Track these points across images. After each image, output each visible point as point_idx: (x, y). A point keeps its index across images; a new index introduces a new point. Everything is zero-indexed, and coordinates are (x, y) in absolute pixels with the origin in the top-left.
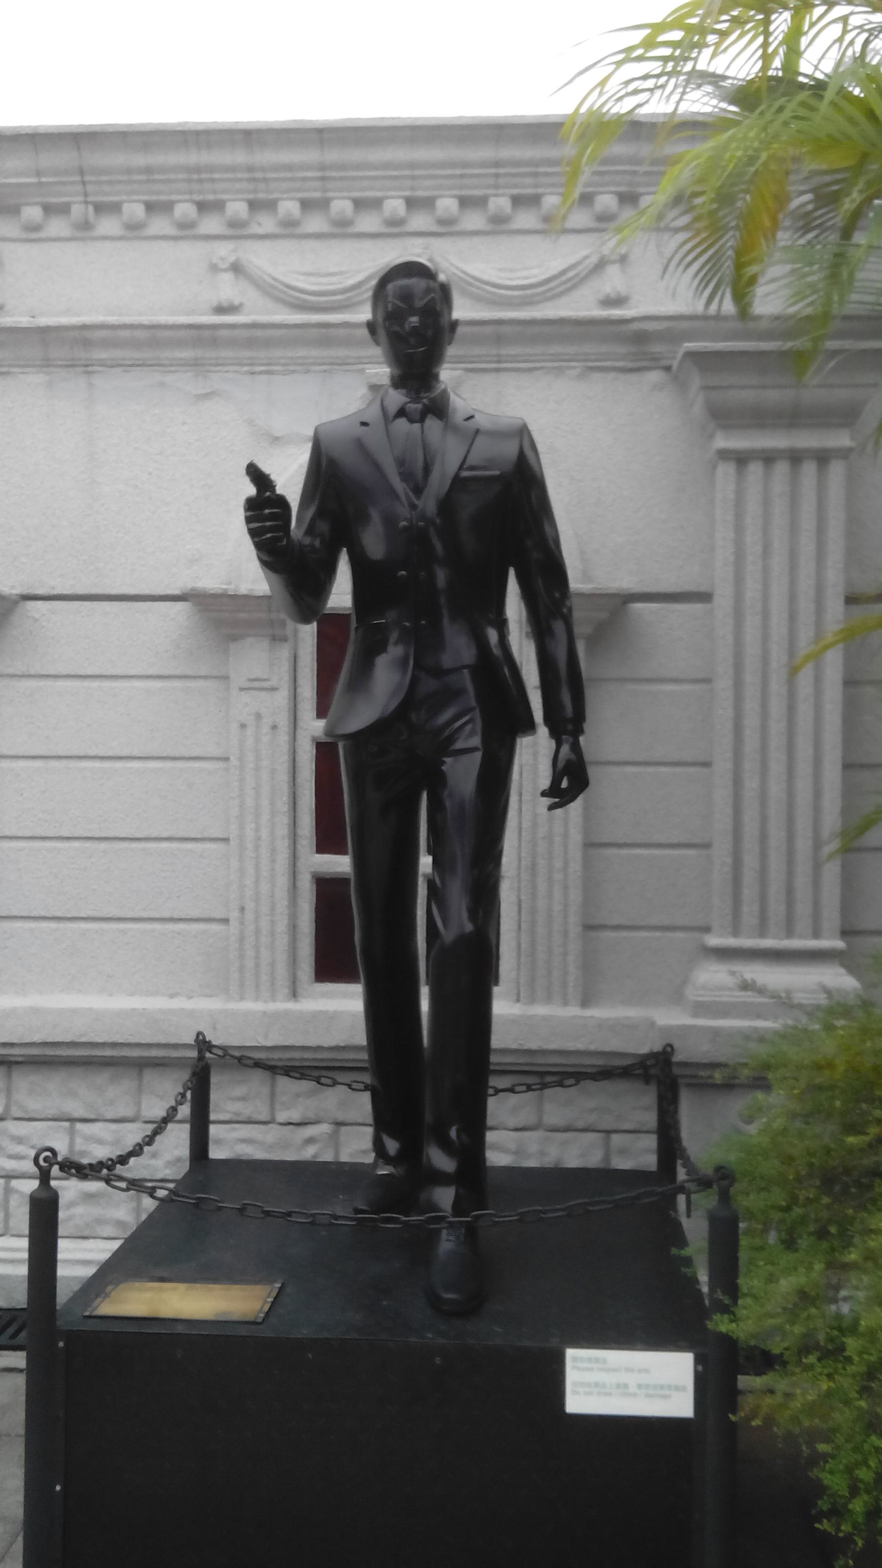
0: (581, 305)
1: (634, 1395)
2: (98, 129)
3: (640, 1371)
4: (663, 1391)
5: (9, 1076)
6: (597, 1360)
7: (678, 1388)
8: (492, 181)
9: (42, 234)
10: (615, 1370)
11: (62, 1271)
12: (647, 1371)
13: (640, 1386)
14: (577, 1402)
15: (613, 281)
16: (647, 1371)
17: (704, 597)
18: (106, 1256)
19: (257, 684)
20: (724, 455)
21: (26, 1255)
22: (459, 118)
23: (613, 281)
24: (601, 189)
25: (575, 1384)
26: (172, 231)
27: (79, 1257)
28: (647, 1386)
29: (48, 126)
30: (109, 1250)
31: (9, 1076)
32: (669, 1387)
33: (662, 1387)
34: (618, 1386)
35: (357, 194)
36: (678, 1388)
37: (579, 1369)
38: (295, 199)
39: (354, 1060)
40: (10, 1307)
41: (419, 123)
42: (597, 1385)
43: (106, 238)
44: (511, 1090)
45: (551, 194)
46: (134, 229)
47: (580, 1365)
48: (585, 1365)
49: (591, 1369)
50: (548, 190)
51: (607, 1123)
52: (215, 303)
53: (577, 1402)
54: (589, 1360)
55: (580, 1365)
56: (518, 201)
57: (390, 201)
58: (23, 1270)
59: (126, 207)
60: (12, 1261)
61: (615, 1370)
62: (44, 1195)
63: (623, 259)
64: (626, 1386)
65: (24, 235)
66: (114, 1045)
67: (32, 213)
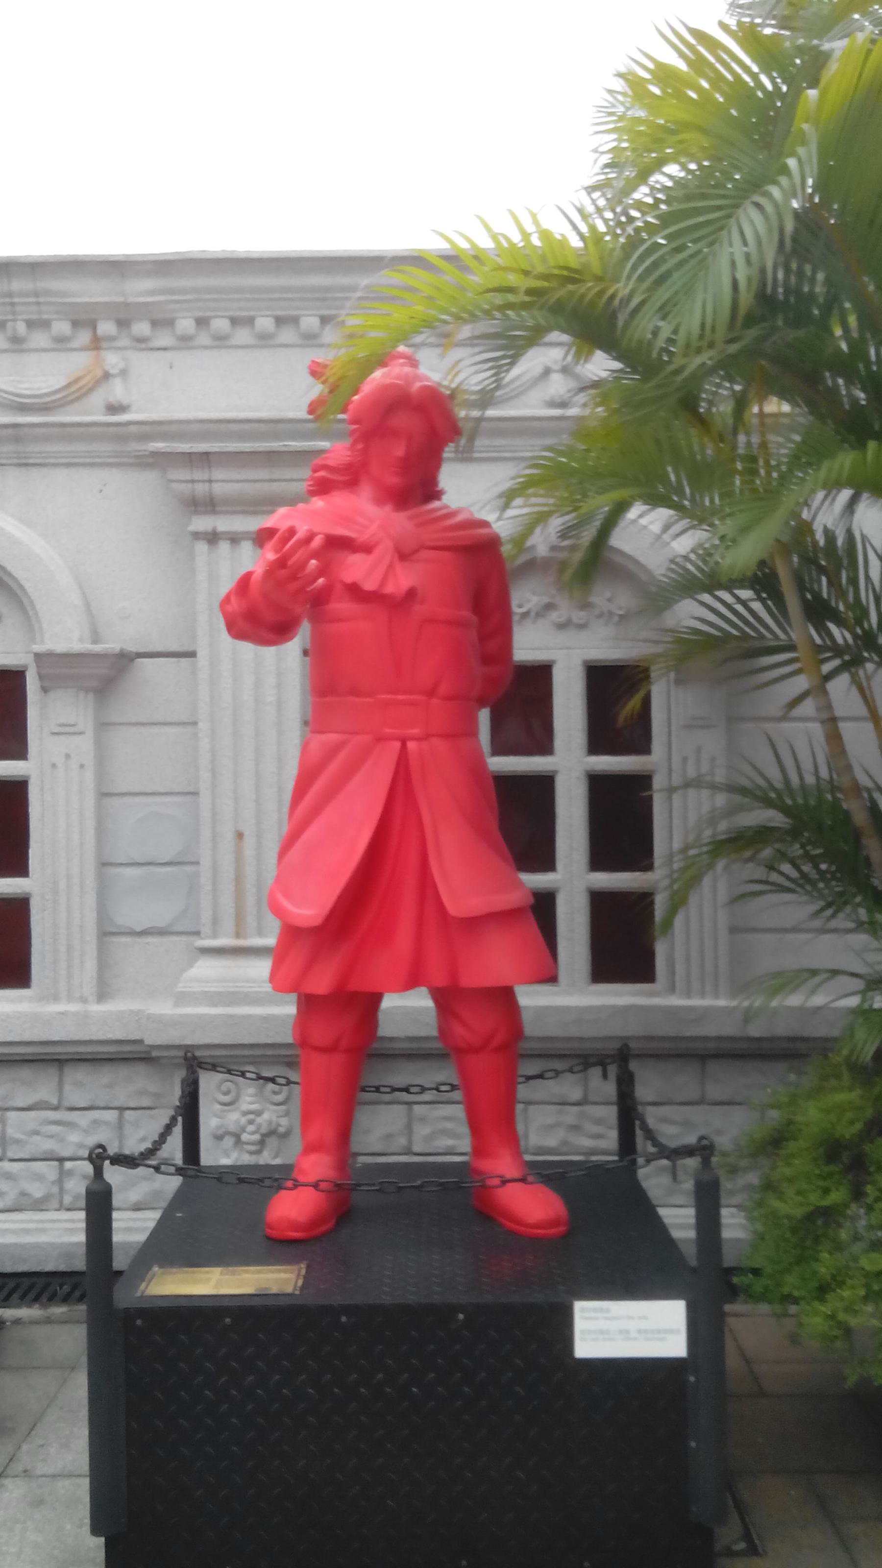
0: (91, 411)
1: (635, 1339)
2: (171, 258)
3: (640, 1318)
4: (662, 1333)
5: (61, 1071)
6: (601, 1310)
7: (672, 1331)
8: (9, 308)
9: (228, 343)
10: (616, 1318)
11: (116, 1238)
12: (645, 1317)
13: (640, 1331)
14: (585, 1347)
15: (117, 391)
16: (645, 1317)
17: (192, 654)
18: (152, 1225)
19: (68, 729)
20: (196, 536)
21: (83, 1225)
22: (368, 250)
23: (117, 391)
24: (212, 314)
25: (582, 1332)
26: (251, 341)
27: (131, 1227)
28: (646, 1331)
29: (94, 256)
30: (153, 1220)
31: (61, 1071)
32: (666, 1331)
33: (659, 1331)
34: (621, 1332)
35: (279, 313)
36: (672, 1331)
37: (587, 1318)
38: (190, 317)
39: (131, 1052)
40: (69, 1270)
41: (304, 255)
42: (602, 1332)
43: (37, 350)
44: (540, 1076)
45: (184, 318)
46: (265, 340)
47: (587, 1315)
48: (593, 1315)
49: (596, 1318)
50: (262, 313)
51: (121, 1099)
52: (547, 398)
53: (585, 1347)
54: (595, 1310)
55: (587, 1315)
56: (235, 322)
57: (217, 320)
58: (81, 1238)
59: (9, 325)
60: (72, 1230)
61: (616, 1318)
62: (96, 1187)
63: (124, 373)
64: (627, 1332)
65: (54, 346)
66: (91, 1042)
67: (142, 328)
